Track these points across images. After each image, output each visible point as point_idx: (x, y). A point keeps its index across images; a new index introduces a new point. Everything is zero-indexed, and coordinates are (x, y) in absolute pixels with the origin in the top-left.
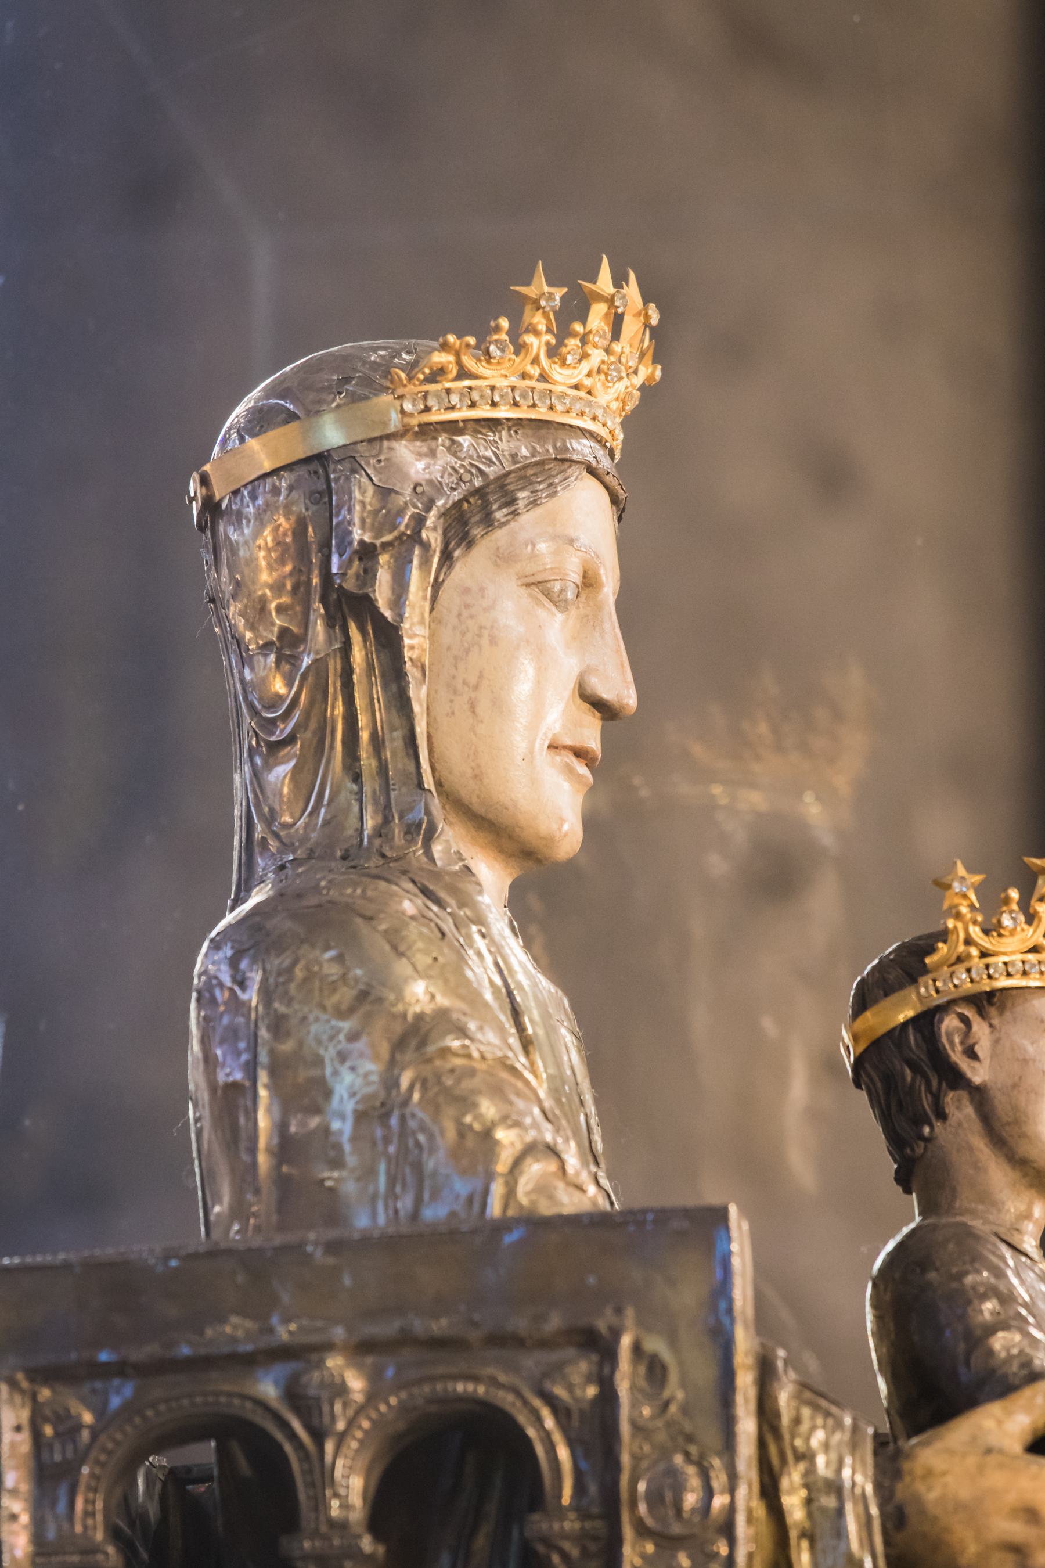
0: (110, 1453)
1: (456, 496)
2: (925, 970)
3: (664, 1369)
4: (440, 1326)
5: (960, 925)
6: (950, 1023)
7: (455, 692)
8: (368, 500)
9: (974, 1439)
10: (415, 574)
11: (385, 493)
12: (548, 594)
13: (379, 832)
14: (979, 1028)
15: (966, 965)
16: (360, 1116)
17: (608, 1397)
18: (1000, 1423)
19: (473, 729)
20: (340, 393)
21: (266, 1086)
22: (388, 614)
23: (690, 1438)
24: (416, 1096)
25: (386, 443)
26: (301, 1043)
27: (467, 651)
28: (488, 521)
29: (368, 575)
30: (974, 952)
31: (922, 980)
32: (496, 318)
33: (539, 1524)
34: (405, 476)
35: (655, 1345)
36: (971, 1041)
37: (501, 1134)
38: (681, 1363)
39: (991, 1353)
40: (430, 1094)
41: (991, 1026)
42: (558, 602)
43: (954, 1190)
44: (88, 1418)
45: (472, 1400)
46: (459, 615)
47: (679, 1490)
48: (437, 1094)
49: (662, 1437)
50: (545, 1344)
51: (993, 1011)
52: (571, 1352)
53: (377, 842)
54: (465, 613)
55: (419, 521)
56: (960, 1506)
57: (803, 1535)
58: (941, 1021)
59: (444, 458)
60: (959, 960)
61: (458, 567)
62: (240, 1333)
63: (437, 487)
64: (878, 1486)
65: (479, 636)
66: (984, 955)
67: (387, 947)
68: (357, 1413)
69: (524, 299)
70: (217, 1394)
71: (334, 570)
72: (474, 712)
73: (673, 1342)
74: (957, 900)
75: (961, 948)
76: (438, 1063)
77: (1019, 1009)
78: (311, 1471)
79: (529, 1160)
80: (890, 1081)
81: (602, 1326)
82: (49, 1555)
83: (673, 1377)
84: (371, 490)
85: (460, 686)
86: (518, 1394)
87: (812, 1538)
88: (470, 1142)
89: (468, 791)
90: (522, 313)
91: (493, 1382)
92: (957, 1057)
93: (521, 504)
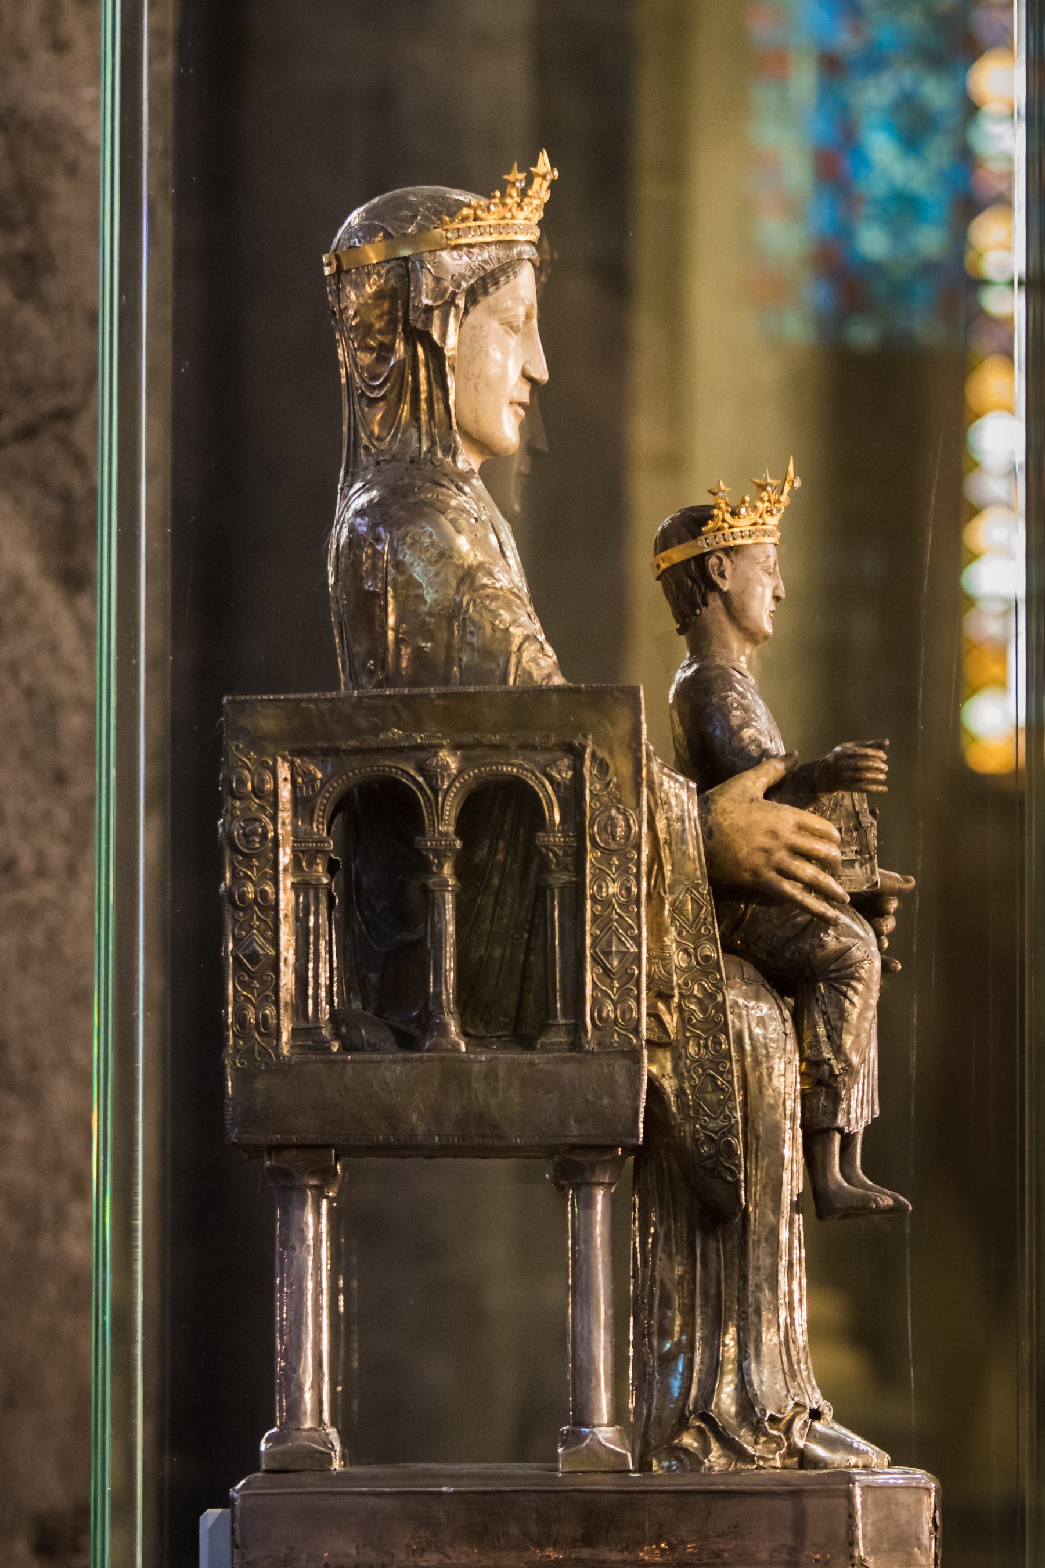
0: (330, 793)
1: (472, 281)
2: (702, 534)
4: (497, 738)
5: (720, 513)
6: (713, 560)
7: (468, 379)
8: (429, 283)
9: (744, 792)
10: (452, 320)
11: (438, 280)
12: (512, 328)
13: (429, 450)
14: (726, 562)
15: (722, 532)
17: (578, 779)
18: (754, 783)
19: (476, 398)
20: (412, 224)
22: (438, 342)
23: (619, 801)
25: (438, 252)
27: (474, 359)
28: (486, 293)
29: (428, 321)
30: (726, 525)
31: (700, 538)
32: (494, 192)
33: (542, 838)
34: (447, 272)
35: (602, 754)
36: (722, 569)
39: (742, 739)
40: (478, 608)
41: (731, 561)
42: (515, 330)
43: (710, 641)
44: (319, 775)
45: (510, 775)
46: (471, 341)
47: (614, 826)
48: (481, 608)
49: (606, 799)
50: (546, 749)
51: (732, 553)
52: (559, 754)
53: (429, 456)
54: (474, 339)
55: (454, 295)
56: (740, 829)
57: (666, 843)
58: (709, 559)
59: (465, 258)
60: (719, 530)
61: (470, 316)
62: (396, 737)
63: (463, 277)
64: (700, 816)
66: (731, 527)
67: (452, 529)
68: (454, 780)
69: (507, 182)
70: (384, 767)
72: (477, 390)
73: (611, 753)
74: (720, 501)
75: (720, 524)
76: (481, 592)
77: (745, 553)
78: (431, 807)
79: (526, 644)
80: (679, 583)
81: (576, 742)
82: (300, 842)
83: (611, 770)
84: (430, 278)
85: (470, 377)
86: (534, 774)
87: (670, 845)
88: (498, 635)
89: (471, 427)
90: (506, 188)
91: (521, 766)
92: (716, 578)
93: (501, 283)
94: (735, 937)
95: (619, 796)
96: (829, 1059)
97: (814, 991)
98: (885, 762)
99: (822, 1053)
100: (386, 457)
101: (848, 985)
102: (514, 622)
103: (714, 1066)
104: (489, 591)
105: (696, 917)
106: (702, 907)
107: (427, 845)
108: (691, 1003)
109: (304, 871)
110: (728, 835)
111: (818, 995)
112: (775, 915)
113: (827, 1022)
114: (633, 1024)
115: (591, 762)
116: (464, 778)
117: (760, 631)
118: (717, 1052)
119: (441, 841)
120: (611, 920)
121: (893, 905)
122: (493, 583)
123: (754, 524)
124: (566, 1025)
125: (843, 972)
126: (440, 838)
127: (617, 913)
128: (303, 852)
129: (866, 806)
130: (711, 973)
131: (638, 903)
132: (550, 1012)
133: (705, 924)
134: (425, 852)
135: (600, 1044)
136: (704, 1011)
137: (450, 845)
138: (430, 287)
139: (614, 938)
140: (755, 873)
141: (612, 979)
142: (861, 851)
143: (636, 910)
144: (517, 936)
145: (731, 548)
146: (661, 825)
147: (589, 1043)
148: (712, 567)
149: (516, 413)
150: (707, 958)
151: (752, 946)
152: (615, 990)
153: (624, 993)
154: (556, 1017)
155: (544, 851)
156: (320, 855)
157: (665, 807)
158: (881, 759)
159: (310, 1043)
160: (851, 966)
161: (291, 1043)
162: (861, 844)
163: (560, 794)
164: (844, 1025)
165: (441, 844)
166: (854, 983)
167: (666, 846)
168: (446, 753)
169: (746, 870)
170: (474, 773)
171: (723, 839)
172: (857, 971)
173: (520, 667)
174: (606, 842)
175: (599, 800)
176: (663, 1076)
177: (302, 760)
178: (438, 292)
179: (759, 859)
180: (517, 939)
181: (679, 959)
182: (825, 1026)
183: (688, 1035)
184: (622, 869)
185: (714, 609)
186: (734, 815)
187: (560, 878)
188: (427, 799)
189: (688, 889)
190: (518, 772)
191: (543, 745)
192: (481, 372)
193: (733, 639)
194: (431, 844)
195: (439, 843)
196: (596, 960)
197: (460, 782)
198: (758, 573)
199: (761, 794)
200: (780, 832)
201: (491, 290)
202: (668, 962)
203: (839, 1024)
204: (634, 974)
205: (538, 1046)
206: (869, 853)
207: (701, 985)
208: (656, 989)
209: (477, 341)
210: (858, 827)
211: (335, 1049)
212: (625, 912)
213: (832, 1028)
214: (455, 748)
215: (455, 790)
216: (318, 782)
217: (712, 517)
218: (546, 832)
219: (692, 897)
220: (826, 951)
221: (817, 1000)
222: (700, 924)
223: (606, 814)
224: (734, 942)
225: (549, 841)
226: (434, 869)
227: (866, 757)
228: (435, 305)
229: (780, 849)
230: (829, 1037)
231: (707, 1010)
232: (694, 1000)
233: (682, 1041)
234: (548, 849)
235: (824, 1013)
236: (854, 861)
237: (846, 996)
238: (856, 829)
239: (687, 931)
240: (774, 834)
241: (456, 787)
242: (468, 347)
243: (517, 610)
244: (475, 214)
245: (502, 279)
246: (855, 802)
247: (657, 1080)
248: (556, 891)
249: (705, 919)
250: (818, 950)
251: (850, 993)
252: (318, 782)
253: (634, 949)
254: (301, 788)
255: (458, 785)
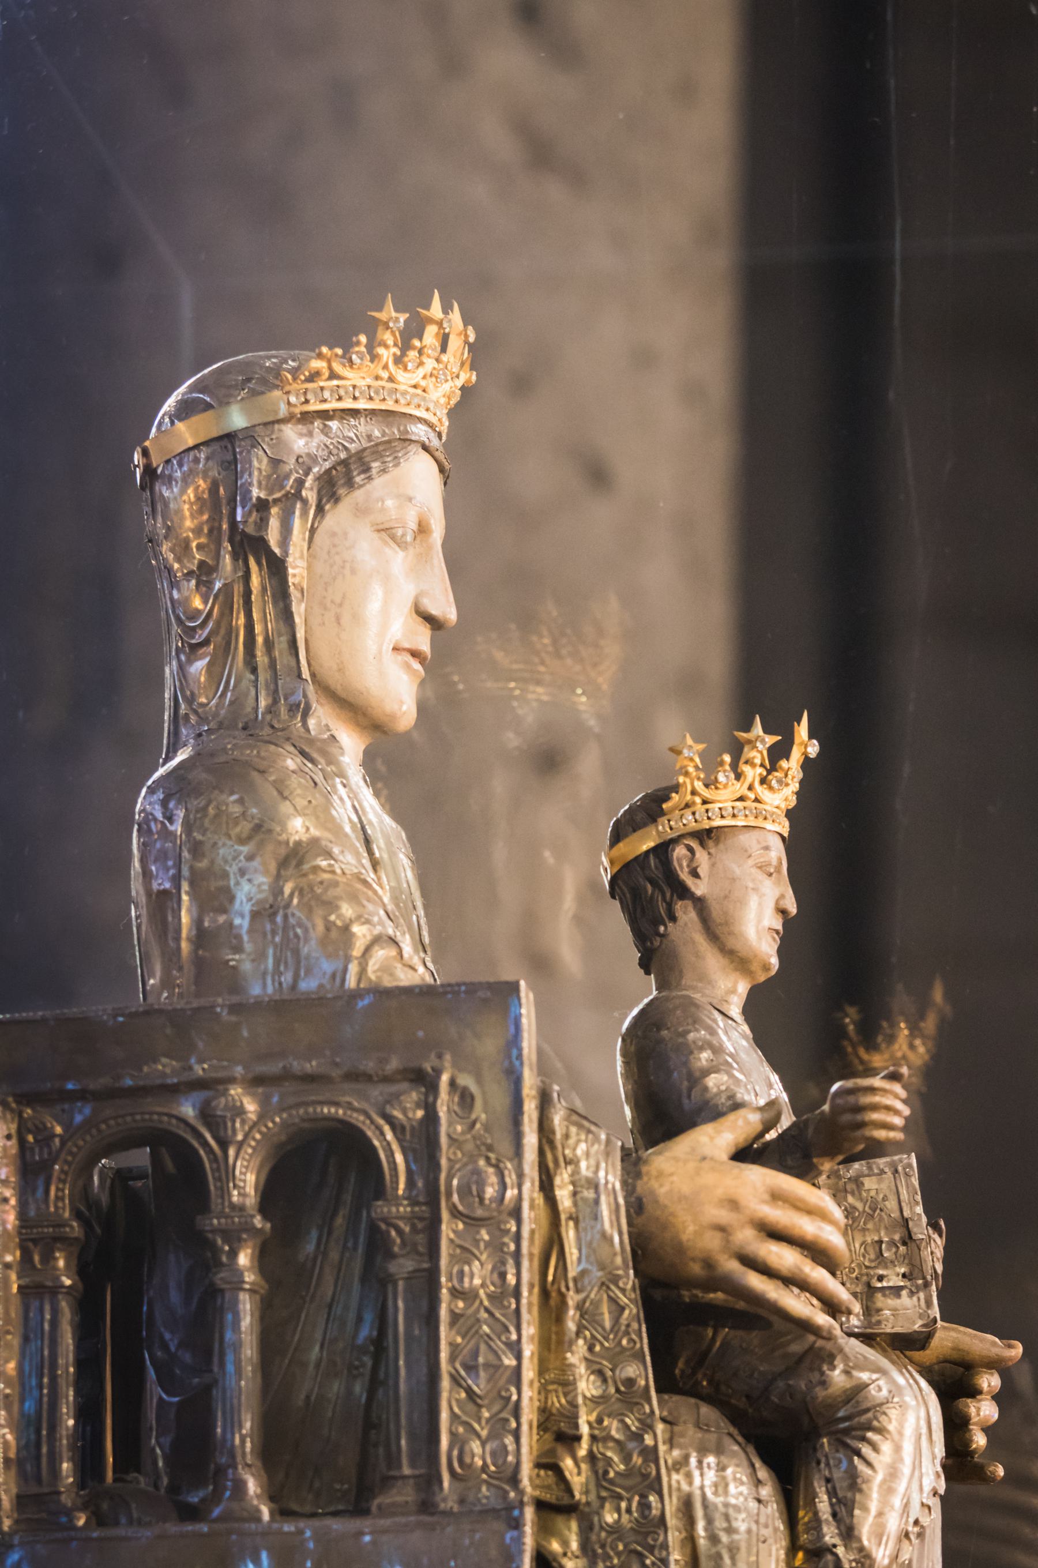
2: (662, 813)
3: (472, 1098)
4: (312, 1066)
5: (688, 781)
6: (679, 852)
7: (325, 609)
8: (263, 467)
9: (693, 1150)
10: (297, 522)
12: (393, 538)
13: (269, 710)
14: (701, 855)
15: (692, 809)
16: (255, 915)
17: (431, 1118)
18: (712, 1138)
21: (187, 893)
22: (277, 551)
24: (295, 901)
26: (212, 862)
27: (334, 579)
29: (263, 523)
30: (698, 800)
31: (660, 820)
32: (357, 335)
33: (381, 1208)
34: (290, 450)
35: (466, 1080)
36: (694, 865)
37: (356, 929)
38: (484, 1093)
39: (706, 1089)
40: (306, 899)
41: (709, 854)
43: (681, 972)
44: (58, 1130)
45: (328, 1118)
46: (329, 552)
49: (469, 1146)
50: (387, 1079)
53: (268, 717)
55: (300, 483)
56: (682, 1198)
57: (570, 1218)
58: (673, 850)
60: (687, 806)
62: (168, 1071)
64: (624, 1183)
65: (343, 567)
68: (251, 1129)
69: (377, 321)
71: (239, 518)
72: (339, 623)
75: (689, 797)
78: (218, 1169)
81: (428, 1067)
82: (31, 1227)
85: (329, 605)
88: (334, 934)
89: (334, 680)
91: (350, 1106)
92: (684, 876)
93: (374, 471)
94: (699, 1376)
95: (489, 1141)
96: (835, 1546)
97: (815, 1450)
98: (905, 1102)
99: (824, 1536)
100: (213, 725)
101: (864, 1439)
102: (359, 918)
103: (639, 1538)
104: (326, 876)
105: (616, 1321)
106: (622, 1309)
107: (212, 1224)
108: (607, 1448)
109: (34, 1267)
110: (666, 1206)
111: (819, 1455)
112: (756, 1342)
113: (832, 1493)
114: (509, 1472)
115: (449, 1094)
116: (266, 1126)
117: (756, 956)
118: (644, 1517)
119: (232, 1217)
120: (478, 1320)
121: (990, 1381)
122: (330, 865)
123: (741, 799)
124: (415, 1477)
125: (856, 1420)
126: (233, 1214)
127: (487, 1310)
128: (35, 1241)
129: (919, 1209)
130: (637, 1404)
131: (517, 1293)
132: (393, 1460)
133: (627, 1333)
134: (210, 1235)
135: (462, 1501)
136: (627, 1458)
137: (246, 1222)
138: (264, 473)
139: (483, 1347)
140: (709, 1264)
141: (480, 1406)
142: (911, 1274)
143: (514, 1306)
144: (357, 1363)
145: (709, 831)
146: (563, 1195)
147: (445, 1500)
148: (679, 860)
149: (408, 666)
150: (630, 1382)
151: (723, 1388)
152: (483, 1422)
153: (498, 1427)
154: (399, 1466)
155: (383, 1226)
156: (58, 1245)
157: (570, 1168)
158: (896, 1096)
159: (44, 1515)
160: (868, 1410)
161: (16, 1515)
162: (911, 1265)
163: (405, 1144)
164: (858, 1497)
165: (233, 1222)
166: (870, 1435)
167: (571, 1224)
168: (240, 1090)
169: (693, 1259)
170: (281, 1118)
171: (658, 1213)
172: (876, 1418)
173: (363, 977)
174: (469, 1206)
175: (460, 1148)
176: (565, 1554)
177: (33, 1109)
178: (276, 480)
179: (712, 1242)
180: (357, 1368)
181: (587, 1386)
182: (830, 1499)
183: (604, 1494)
184: (497, 1247)
185: (686, 924)
186: (675, 1178)
187: (403, 1266)
188: (214, 1159)
189: (603, 1284)
190: (345, 1114)
191: (380, 1073)
192: (344, 597)
193: (712, 962)
194: (219, 1223)
195: (229, 1221)
196: (455, 1380)
197: (260, 1132)
198: (745, 870)
199: (724, 1156)
200: (743, 1202)
201: (358, 479)
202: (571, 1388)
203: (849, 1495)
204: (509, 1398)
205: (374, 1508)
206: (924, 1278)
207: (622, 1422)
208: (555, 1428)
209: (337, 553)
210: (908, 1239)
211: (81, 1522)
212: (498, 1308)
213: (839, 1501)
214: (256, 1082)
215: (253, 1143)
216: (57, 1141)
217: (676, 788)
218: (386, 1200)
219: (609, 1297)
220: (830, 1391)
221: (818, 1463)
222: (620, 1334)
223: (470, 1167)
224: (698, 1383)
225: (389, 1212)
226: (224, 1259)
227: (872, 1090)
228: (270, 498)
229: (743, 1227)
230: (834, 1515)
231: (631, 1459)
232: (611, 1444)
233: (596, 1504)
234: (389, 1224)
235: (828, 1480)
236: (902, 1288)
237: (858, 1453)
238: (904, 1243)
239: (602, 1344)
240: (733, 1204)
241: (254, 1139)
242: (325, 561)
243: (365, 903)
244: (330, 368)
245: (375, 465)
246: (903, 1204)
247: (555, 1560)
248: (401, 1284)
249: (628, 1326)
250: (817, 1389)
251: (866, 1450)
252: (57, 1141)
253: (509, 1361)
254: (32, 1150)
255: (258, 1136)
